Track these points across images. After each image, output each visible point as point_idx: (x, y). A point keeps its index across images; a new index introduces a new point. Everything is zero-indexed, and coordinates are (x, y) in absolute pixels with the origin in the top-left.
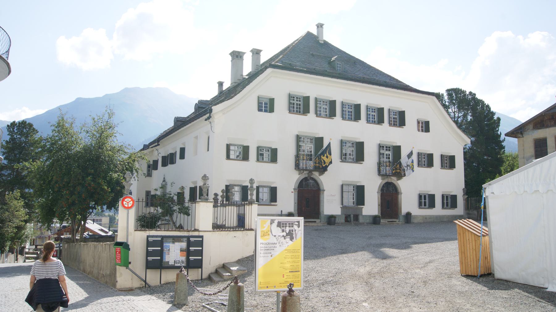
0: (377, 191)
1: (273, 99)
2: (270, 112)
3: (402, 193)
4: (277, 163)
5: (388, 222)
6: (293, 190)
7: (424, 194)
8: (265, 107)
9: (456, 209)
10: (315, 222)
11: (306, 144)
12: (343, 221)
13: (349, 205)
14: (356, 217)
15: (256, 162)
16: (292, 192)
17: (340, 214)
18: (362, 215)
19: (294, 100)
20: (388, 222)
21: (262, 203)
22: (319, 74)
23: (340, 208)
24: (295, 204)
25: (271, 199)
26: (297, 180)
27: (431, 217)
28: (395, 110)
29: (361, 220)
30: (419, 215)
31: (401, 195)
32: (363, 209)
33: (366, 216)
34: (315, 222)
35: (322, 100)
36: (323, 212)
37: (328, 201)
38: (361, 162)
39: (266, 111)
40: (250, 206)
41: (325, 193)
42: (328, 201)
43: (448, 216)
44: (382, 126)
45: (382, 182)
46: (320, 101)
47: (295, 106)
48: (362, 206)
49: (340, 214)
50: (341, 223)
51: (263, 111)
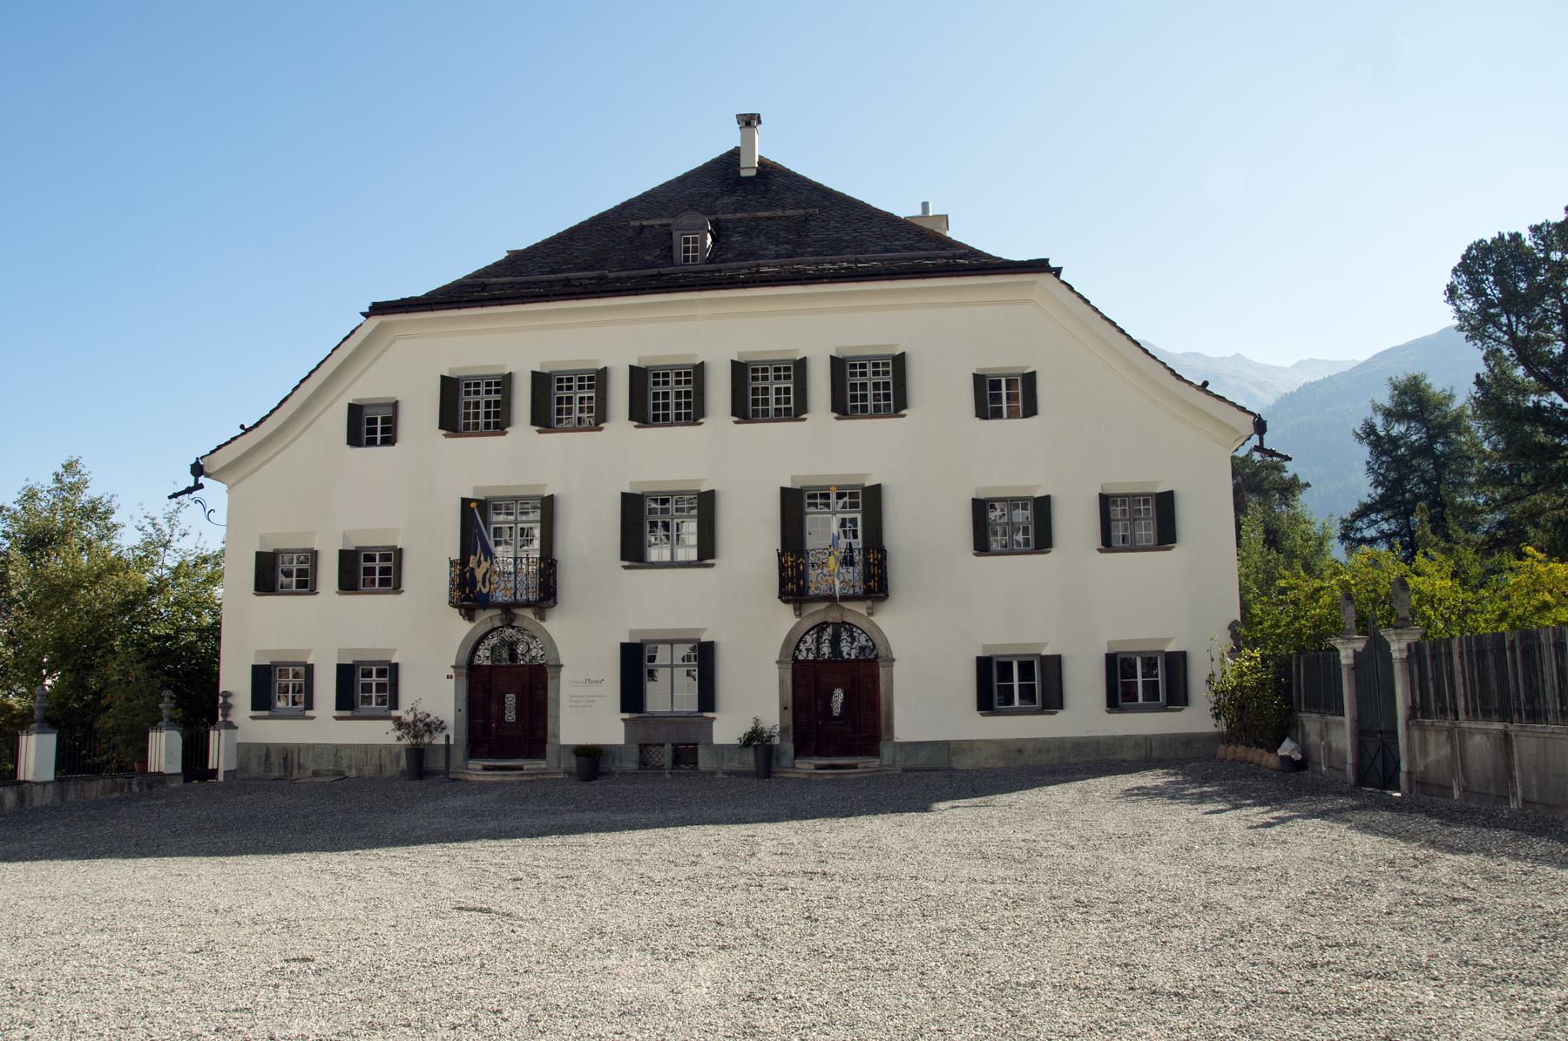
0: (777, 658)
1: (1033, 374)
2: (1025, 416)
3: (893, 660)
4: (403, 591)
5: (486, 768)
6: (451, 672)
7: (1022, 655)
8: (374, 431)
9: (1187, 710)
10: (855, 767)
11: (516, 524)
12: (631, 765)
13: (675, 710)
14: (685, 755)
15: (337, 595)
16: (448, 677)
17: (623, 742)
18: (710, 743)
19: (863, 374)
20: (818, 767)
21: (362, 713)
22: (437, 304)
23: (623, 724)
24: (459, 714)
25: (642, 694)
26: (466, 639)
27: (1043, 745)
28: (684, 366)
29: (705, 761)
30: (985, 741)
31: (892, 666)
32: (715, 724)
33: (722, 746)
34: (855, 767)
35: (672, 370)
36: (557, 736)
37: (574, 699)
38: (709, 561)
39: (1013, 414)
40: (158, 734)
41: (565, 675)
42: (574, 699)
43: (1146, 738)
44: (702, 426)
45: (798, 624)
46: (785, 368)
47: (870, 392)
48: (709, 715)
49: (623, 742)
50: (620, 774)
51: (379, 442)
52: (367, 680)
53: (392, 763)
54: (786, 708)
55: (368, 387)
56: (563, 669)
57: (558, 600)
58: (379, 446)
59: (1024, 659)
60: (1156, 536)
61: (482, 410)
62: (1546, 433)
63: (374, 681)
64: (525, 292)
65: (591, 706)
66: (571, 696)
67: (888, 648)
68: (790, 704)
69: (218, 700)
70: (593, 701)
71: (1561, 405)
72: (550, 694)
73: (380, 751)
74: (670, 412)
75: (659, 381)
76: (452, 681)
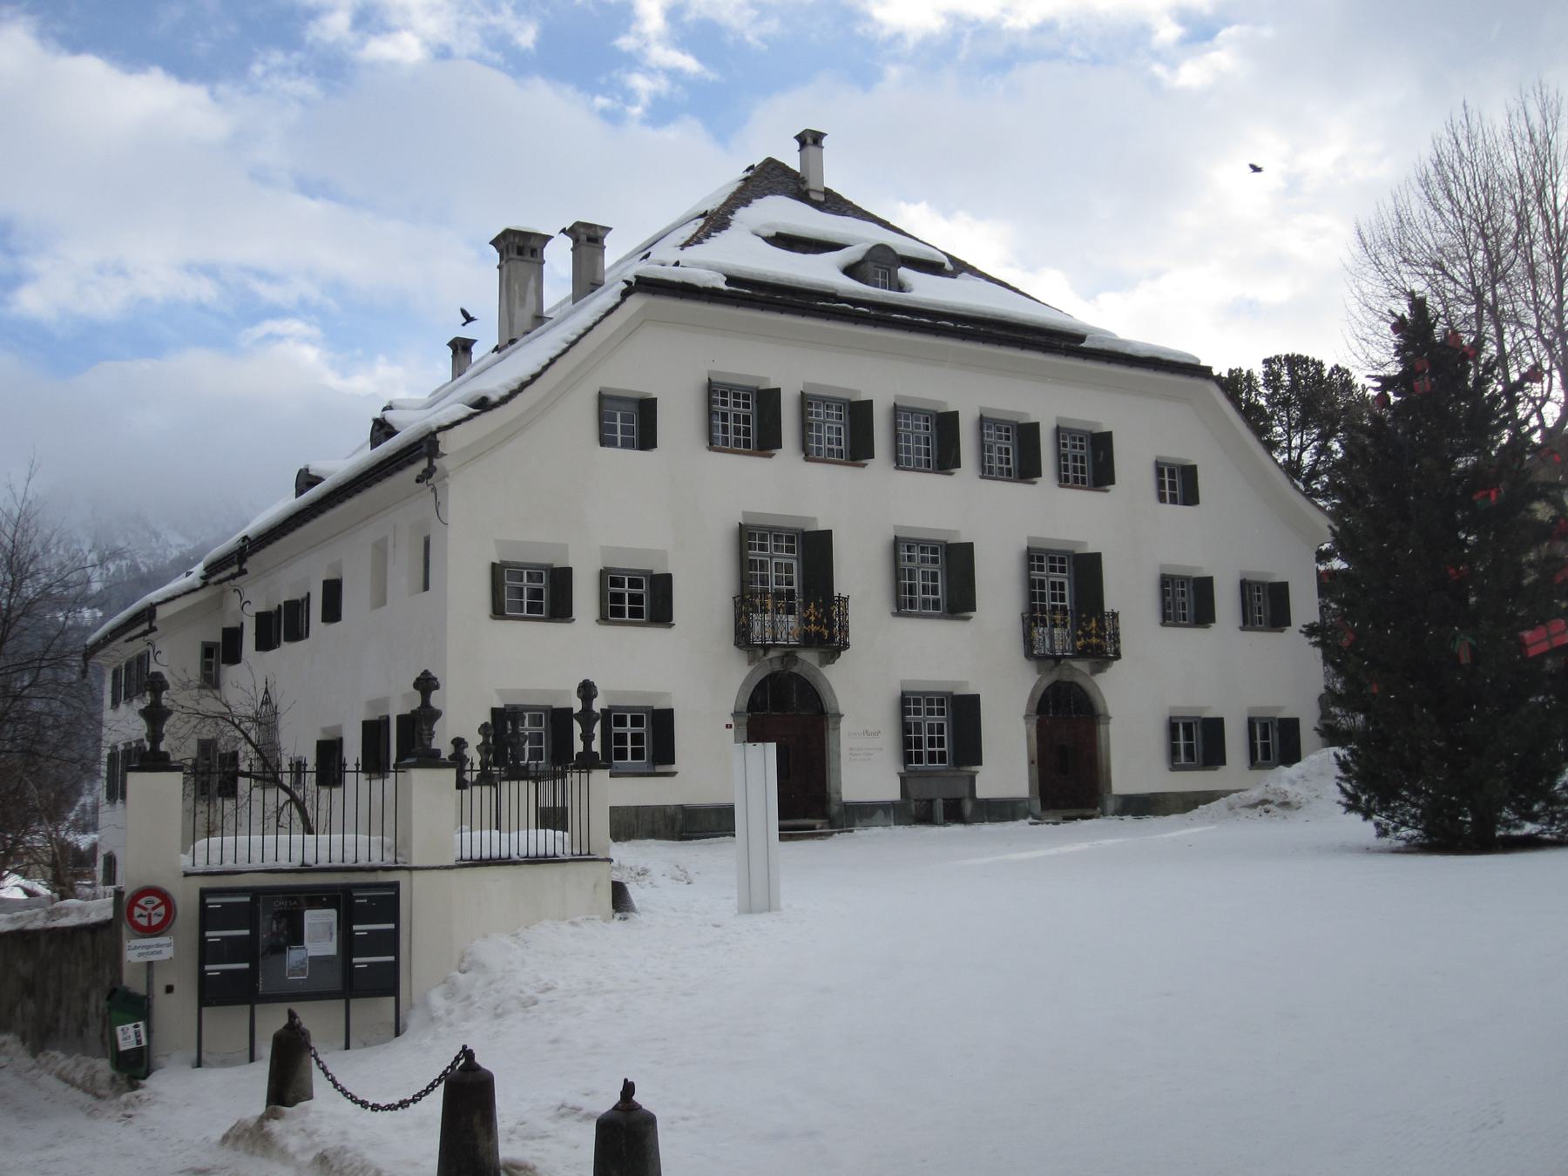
6: (730, 721)
16: (727, 726)
36: (839, 792)
41: (844, 725)
52: (637, 730)
53: (666, 826)
54: (1033, 762)
55: (629, 379)
56: (843, 719)
57: (1021, 617)
58: (619, 448)
59: (1187, 721)
60: (951, 740)
61: (731, 424)
62: (1366, 800)
63: (628, 730)
64: (799, 303)
65: (869, 759)
66: (851, 749)
67: (1105, 708)
68: (1036, 758)
69: (1339, 571)
70: (871, 755)
71: (1284, 459)
72: (831, 745)
73: (653, 814)
74: (729, 424)
75: (1076, 462)
76: (731, 731)
